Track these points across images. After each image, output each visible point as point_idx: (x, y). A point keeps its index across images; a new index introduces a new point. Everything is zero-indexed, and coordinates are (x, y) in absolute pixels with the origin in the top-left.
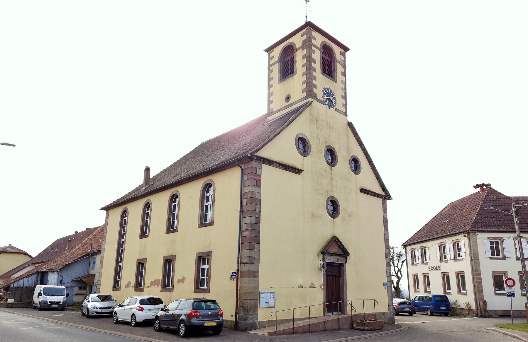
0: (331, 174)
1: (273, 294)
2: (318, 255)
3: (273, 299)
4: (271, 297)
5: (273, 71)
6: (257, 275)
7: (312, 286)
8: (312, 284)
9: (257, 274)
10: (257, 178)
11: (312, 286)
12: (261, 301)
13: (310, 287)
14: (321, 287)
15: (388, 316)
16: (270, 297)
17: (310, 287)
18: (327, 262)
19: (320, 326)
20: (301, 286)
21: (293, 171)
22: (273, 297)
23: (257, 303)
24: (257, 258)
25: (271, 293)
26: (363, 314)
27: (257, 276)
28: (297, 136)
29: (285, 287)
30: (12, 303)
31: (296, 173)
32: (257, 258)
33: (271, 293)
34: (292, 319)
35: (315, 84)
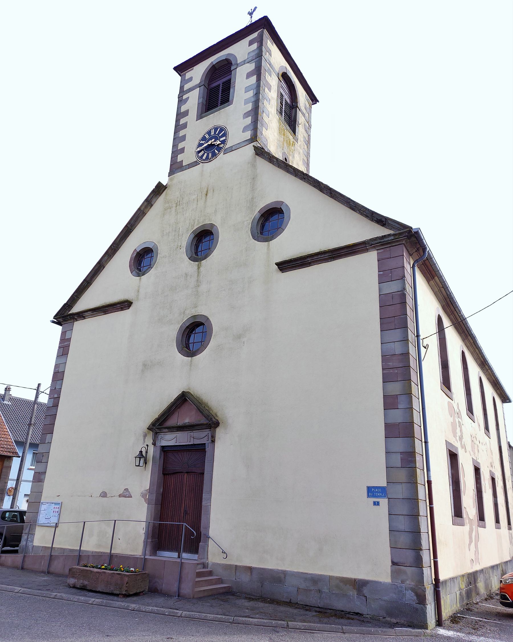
0: (198, 276)
1: (58, 506)
2: (145, 436)
3: (57, 514)
4: (55, 510)
5: (185, 140)
6: (42, 478)
7: (126, 494)
8: (126, 490)
9: (42, 477)
10: (64, 344)
11: (126, 494)
12: (41, 516)
13: (120, 496)
14: (143, 496)
15: (386, 598)
16: (53, 510)
17: (120, 496)
18: (163, 447)
19: (41, 563)
20: (104, 495)
21: (116, 309)
22: (57, 510)
23: (36, 517)
24: (46, 454)
25: (55, 504)
26: (76, 550)
27: (42, 479)
28: (135, 250)
29: (79, 496)
30: (28, 505)
31: (122, 309)
32: (46, 454)
33: (55, 504)
34: (48, 547)
35: (186, 139)
